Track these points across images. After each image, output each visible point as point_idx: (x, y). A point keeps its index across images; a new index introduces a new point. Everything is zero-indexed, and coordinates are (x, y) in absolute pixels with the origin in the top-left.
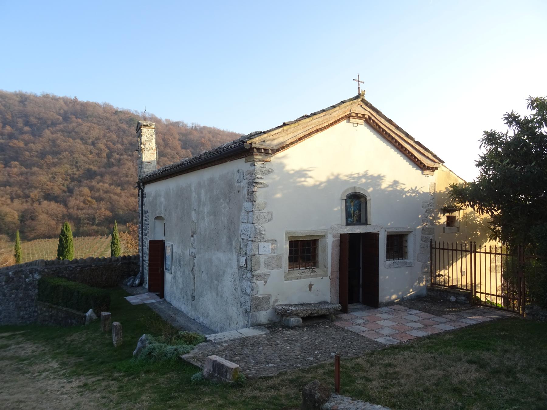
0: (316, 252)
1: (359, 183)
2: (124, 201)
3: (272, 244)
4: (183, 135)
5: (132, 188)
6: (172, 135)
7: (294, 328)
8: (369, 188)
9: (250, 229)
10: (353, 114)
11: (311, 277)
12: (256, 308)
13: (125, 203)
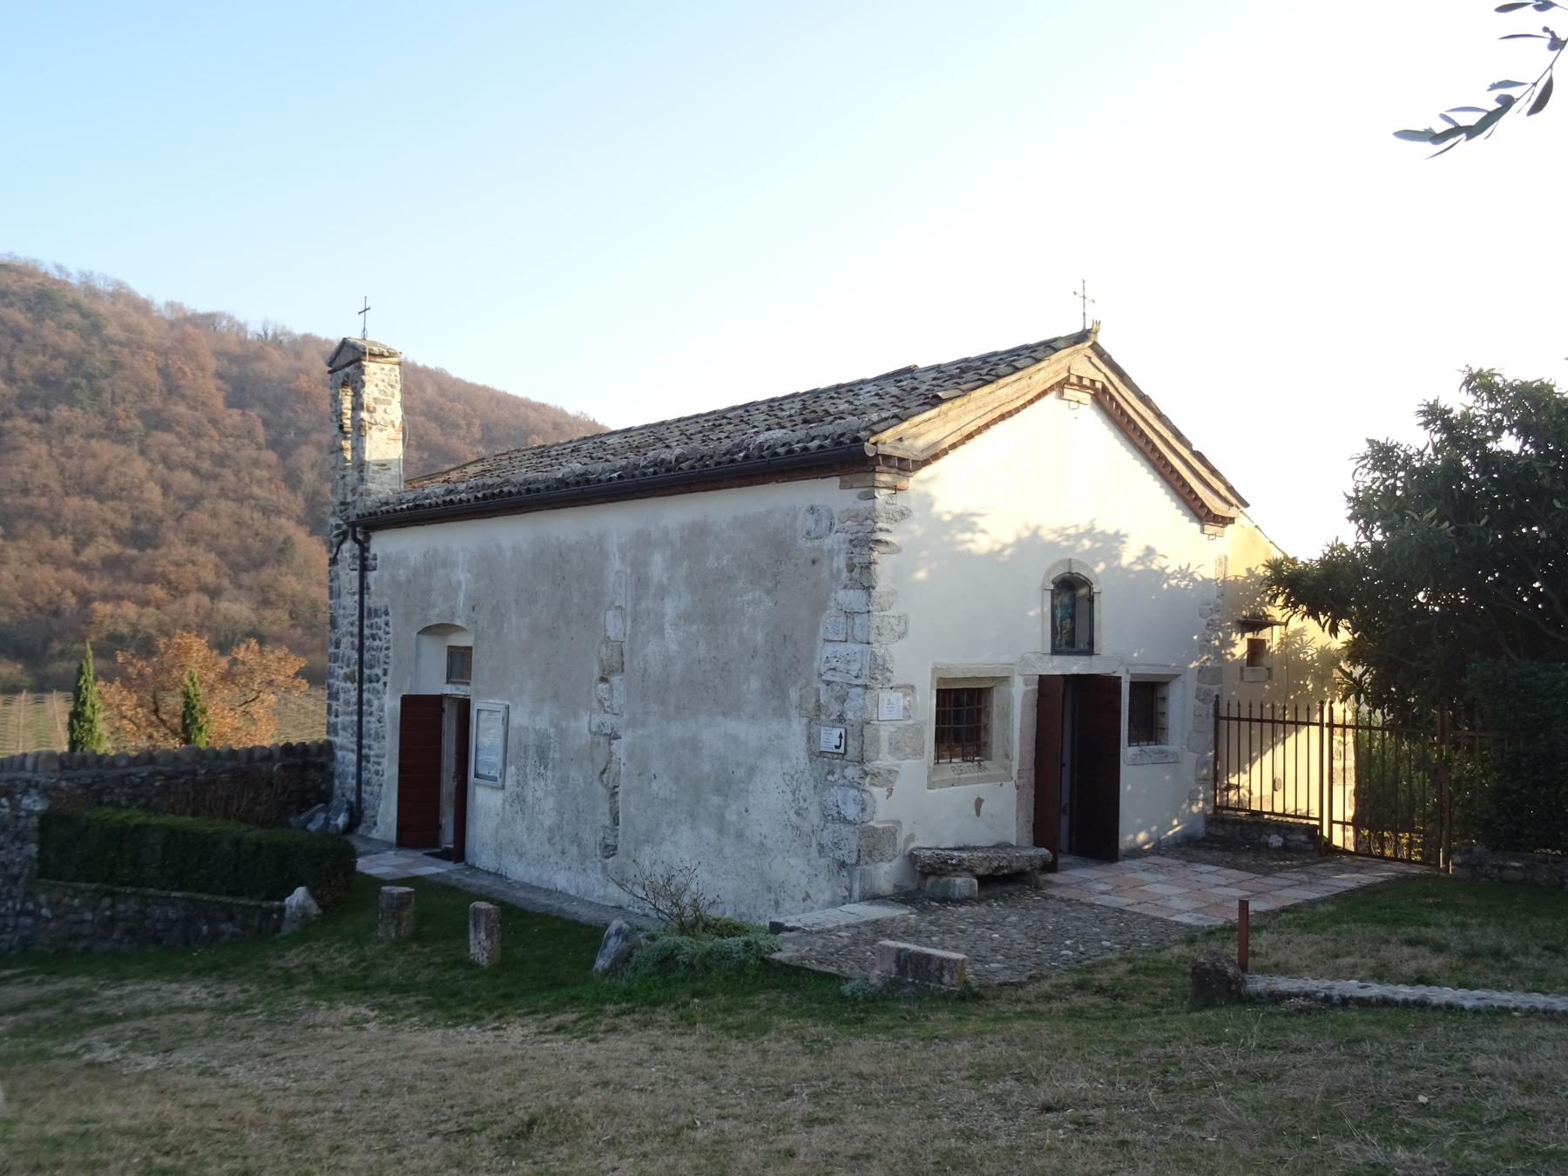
0: (983, 720)
2: (17, 578)
3: (905, 695)
4: (233, 359)
5: (46, 532)
6: (192, 356)
7: (963, 901)
8: (1096, 564)
9: (858, 656)
10: (1074, 380)
11: (979, 780)
12: (870, 854)
13: (18, 585)
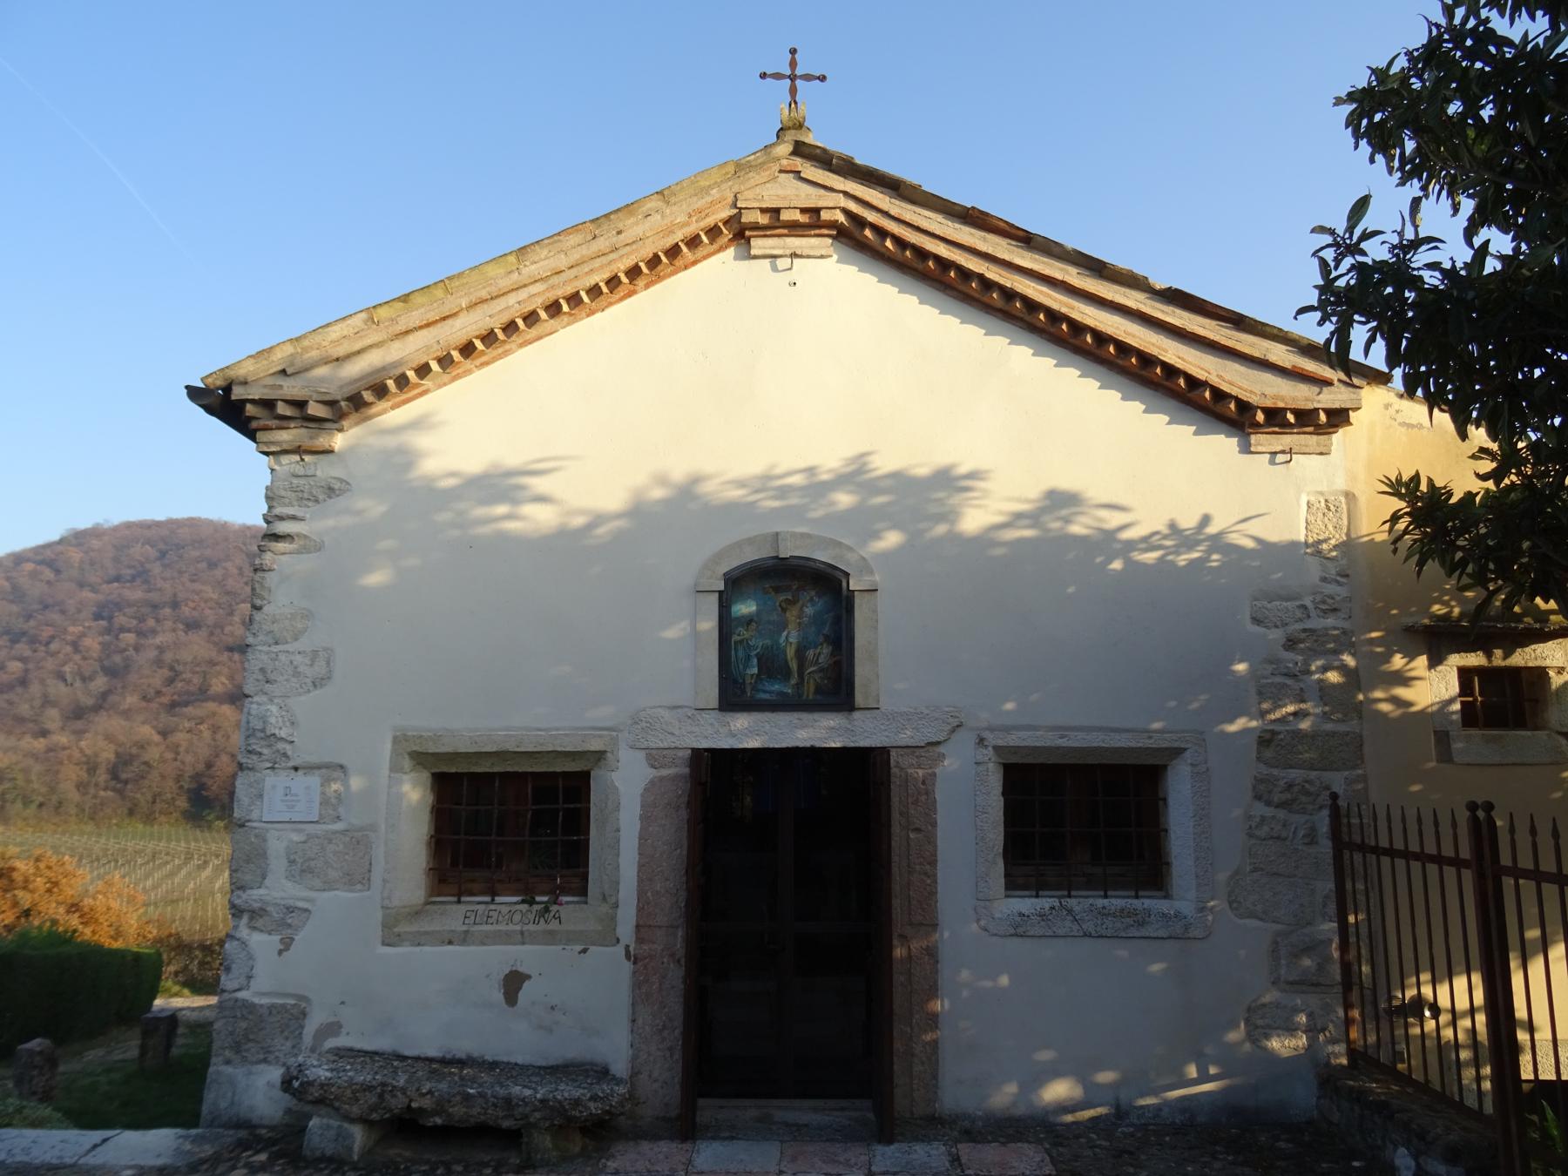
1: (818, 513)
11: (523, 938)
12: (237, 1047)
